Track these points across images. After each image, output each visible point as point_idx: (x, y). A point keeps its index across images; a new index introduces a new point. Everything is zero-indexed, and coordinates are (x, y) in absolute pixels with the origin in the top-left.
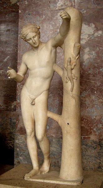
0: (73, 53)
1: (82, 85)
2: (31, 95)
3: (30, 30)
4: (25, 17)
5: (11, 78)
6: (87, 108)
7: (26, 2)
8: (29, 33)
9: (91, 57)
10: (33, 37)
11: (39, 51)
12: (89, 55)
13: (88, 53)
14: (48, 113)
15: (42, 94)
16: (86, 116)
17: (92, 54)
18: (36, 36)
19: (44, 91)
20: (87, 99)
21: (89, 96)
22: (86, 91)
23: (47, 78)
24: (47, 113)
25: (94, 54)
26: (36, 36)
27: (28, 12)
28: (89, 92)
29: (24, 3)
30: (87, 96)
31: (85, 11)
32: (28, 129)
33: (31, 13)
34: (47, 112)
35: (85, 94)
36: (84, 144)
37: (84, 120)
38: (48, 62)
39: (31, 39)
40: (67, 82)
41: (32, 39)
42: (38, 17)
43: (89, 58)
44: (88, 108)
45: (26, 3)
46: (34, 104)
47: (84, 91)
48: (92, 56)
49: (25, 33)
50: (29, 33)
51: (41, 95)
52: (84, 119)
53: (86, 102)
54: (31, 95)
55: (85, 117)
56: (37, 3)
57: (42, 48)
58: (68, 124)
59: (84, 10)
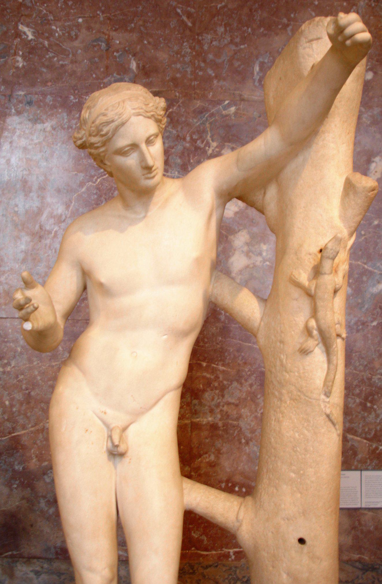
0: (338, 223)
1: (227, 361)
2: (109, 411)
3: (136, 104)
4: (13, 111)
5: (36, 326)
6: (247, 443)
7: (20, 59)
8: (134, 119)
9: (258, 263)
10: (149, 141)
11: (154, 210)
12: (247, 254)
13: (245, 249)
14: (186, 492)
15: (161, 403)
16: (242, 474)
17: (260, 254)
18: (156, 136)
19: (171, 390)
20: (245, 411)
21: (252, 400)
22: (241, 384)
23: (185, 334)
24: (181, 490)
25: (264, 254)
26: (156, 136)
27: (25, 95)
28: (251, 385)
29: (10, 62)
30: (245, 399)
31: (233, 109)
32: (91, 569)
33: (35, 98)
34: (182, 483)
35: (237, 394)
36: (241, 577)
37: (237, 489)
38: (198, 261)
39: (135, 146)
40: (305, 352)
41: (143, 146)
42: (65, 114)
43: (247, 267)
44: (251, 444)
45: (17, 64)
46: (122, 455)
47: (235, 384)
48: (260, 259)
49: (111, 115)
50: (134, 119)
51: (157, 409)
52: (235, 487)
53: (242, 424)
54: (109, 411)
55: (238, 478)
56: (62, 66)
57: (167, 200)
58: (302, 541)
59: (229, 105)
